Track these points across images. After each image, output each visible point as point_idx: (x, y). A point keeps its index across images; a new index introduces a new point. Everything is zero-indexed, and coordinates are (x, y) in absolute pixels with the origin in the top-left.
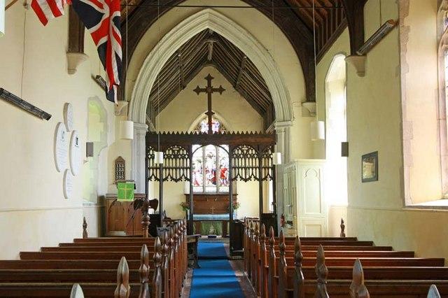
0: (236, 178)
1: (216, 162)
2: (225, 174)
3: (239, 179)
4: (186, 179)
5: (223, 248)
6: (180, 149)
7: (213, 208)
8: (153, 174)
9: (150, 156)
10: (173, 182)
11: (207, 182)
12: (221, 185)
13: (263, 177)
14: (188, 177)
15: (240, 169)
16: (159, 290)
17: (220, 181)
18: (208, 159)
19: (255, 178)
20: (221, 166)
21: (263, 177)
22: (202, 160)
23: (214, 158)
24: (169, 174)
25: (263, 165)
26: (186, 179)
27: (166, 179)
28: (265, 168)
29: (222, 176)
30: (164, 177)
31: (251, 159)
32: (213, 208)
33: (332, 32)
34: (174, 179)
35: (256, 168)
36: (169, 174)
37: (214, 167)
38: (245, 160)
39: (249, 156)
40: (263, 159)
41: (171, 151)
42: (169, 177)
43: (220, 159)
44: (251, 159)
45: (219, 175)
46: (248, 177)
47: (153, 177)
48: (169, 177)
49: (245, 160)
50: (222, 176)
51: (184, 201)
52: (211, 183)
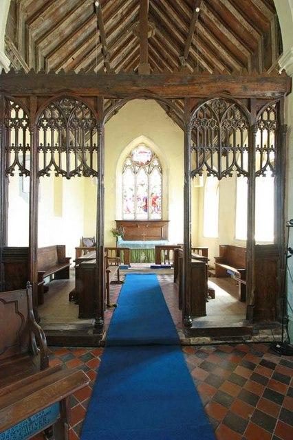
1: (148, 190)
2: (156, 202)
5: (157, 291)
7: (144, 235)
8: (16, 162)
11: (138, 209)
12: (152, 213)
13: (257, 168)
14: (95, 168)
15: (56, 152)
17: (151, 208)
18: (140, 187)
20: (152, 194)
21: (257, 168)
22: (133, 188)
23: (146, 187)
24: (52, 162)
25: (258, 142)
26: (241, 171)
27: (45, 172)
28: (261, 150)
29: (154, 203)
30: (41, 167)
32: (144, 235)
33: (213, 135)
34: (62, 172)
37: (146, 195)
39: (45, 123)
40: (259, 131)
41: (56, 112)
42: (53, 167)
43: (152, 187)
44: (49, 130)
45: (150, 203)
46: (224, 168)
47: (17, 167)
48: (53, 167)
50: (154, 203)
51: (115, 227)
52: (142, 211)
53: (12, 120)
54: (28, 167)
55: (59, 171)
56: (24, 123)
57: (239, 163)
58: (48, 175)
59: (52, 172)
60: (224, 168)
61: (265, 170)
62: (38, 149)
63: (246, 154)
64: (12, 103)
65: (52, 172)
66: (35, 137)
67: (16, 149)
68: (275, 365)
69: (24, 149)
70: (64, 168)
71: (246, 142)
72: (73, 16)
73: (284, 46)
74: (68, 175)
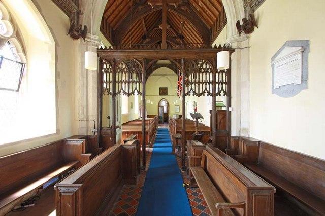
0: (119, 92)
3: (122, 93)
4: (209, 93)
6: (203, 63)
9: (103, 71)
10: (195, 97)
13: (217, 92)
15: (208, 84)
16: (246, 214)
19: (209, 93)
21: (217, 92)
24: (206, 89)
26: (209, 93)
31: (204, 74)
35: (110, 83)
36: (206, 89)
38: (206, 74)
39: (203, 71)
44: (204, 74)
46: (131, 91)
48: (192, 92)
49: (206, 74)
53: (104, 69)
54: (127, 91)
55: (195, 93)
56: (109, 70)
57: (208, 89)
58: (190, 95)
59: (192, 93)
60: (131, 91)
61: (134, 92)
62: (216, 83)
63: (111, 84)
64: (104, 61)
65: (192, 93)
66: (214, 77)
67: (219, 83)
68: (136, 184)
69: (222, 83)
70: (197, 92)
71: (111, 79)
72: (202, 11)
73: (263, 4)
74: (199, 95)
